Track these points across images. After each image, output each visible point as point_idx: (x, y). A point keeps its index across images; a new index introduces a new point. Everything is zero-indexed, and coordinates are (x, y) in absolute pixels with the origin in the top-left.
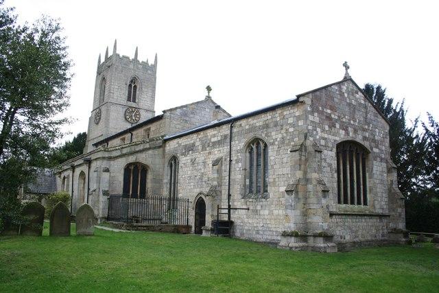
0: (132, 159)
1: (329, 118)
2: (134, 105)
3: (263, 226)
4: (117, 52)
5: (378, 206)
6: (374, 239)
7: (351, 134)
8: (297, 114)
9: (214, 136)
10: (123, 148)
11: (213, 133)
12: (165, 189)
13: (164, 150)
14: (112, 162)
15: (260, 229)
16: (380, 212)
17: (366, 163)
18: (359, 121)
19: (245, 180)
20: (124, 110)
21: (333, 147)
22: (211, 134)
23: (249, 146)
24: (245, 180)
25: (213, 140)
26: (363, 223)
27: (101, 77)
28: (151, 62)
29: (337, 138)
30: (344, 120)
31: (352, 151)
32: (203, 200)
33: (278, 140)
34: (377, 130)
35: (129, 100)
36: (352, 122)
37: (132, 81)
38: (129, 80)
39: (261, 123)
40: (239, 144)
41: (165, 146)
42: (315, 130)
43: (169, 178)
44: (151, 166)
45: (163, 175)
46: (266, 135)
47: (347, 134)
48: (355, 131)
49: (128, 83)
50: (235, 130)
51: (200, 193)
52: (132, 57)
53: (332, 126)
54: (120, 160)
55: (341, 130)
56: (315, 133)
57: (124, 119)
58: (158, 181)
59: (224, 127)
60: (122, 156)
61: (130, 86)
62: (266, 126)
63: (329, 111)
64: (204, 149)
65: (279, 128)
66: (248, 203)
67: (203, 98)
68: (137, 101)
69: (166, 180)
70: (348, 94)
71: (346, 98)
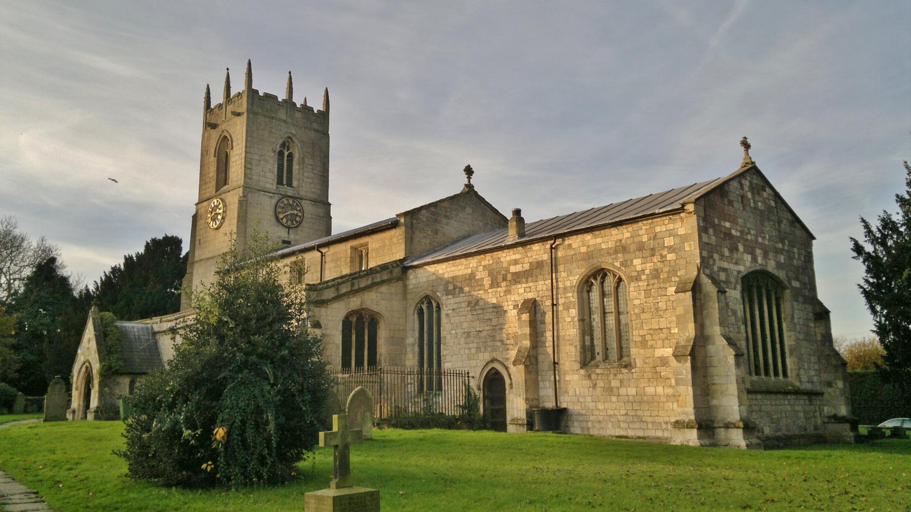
0: (355, 303)
1: (728, 235)
2: (290, 192)
3: (627, 414)
4: (253, 87)
5: (804, 378)
6: (803, 433)
7: (760, 260)
8: (681, 231)
9: (516, 262)
10: (339, 284)
11: (513, 257)
12: (410, 356)
13: (405, 286)
14: (323, 310)
15: (621, 418)
16: (809, 387)
17: (782, 306)
18: (770, 237)
19: (584, 337)
20: (274, 201)
21: (737, 281)
22: (508, 258)
23: (586, 285)
24: (584, 337)
25: (513, 269)
26: (786, 405)
27: (215, 135)
28: (317, 105)
29: (742, 268)
30: (749, 237)
31: (752, 286)
32: (497, 373)
33: (647, 272)
34: (795, 250)
35: (280, 182)
36: (760, 240)
37: (283, 145)
38: (280, 141)
39: (611, 245)
40: (570, 278)
41: (407, 279)
42: (712, 257)
43: (417, 335)
44: (385, 313)
45: (405, 330)
46: (622, 264)
47: (754, 259)
48: (765, 255)
49: (278, 149)
50: (560, 254)
51: (493, 360)
52: (282, 96)
53: (733, 249)
54: (335, 305)
55: (745, 255)
56: (711, 262)
57: (273, 219)
58: (398, 341)
59: (536, 247)
60: (338, 298)
61: (281, 154)
62: (621, 248)
63: (728, 225)
64: (494, 284)
65: (647, 253)
66: (593, 376)
67: (457, 188)
68: (295, 183)
69: (412, 338)
70: (753, 194)
71: (749, 200)
